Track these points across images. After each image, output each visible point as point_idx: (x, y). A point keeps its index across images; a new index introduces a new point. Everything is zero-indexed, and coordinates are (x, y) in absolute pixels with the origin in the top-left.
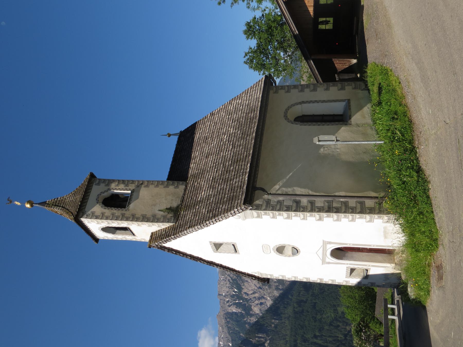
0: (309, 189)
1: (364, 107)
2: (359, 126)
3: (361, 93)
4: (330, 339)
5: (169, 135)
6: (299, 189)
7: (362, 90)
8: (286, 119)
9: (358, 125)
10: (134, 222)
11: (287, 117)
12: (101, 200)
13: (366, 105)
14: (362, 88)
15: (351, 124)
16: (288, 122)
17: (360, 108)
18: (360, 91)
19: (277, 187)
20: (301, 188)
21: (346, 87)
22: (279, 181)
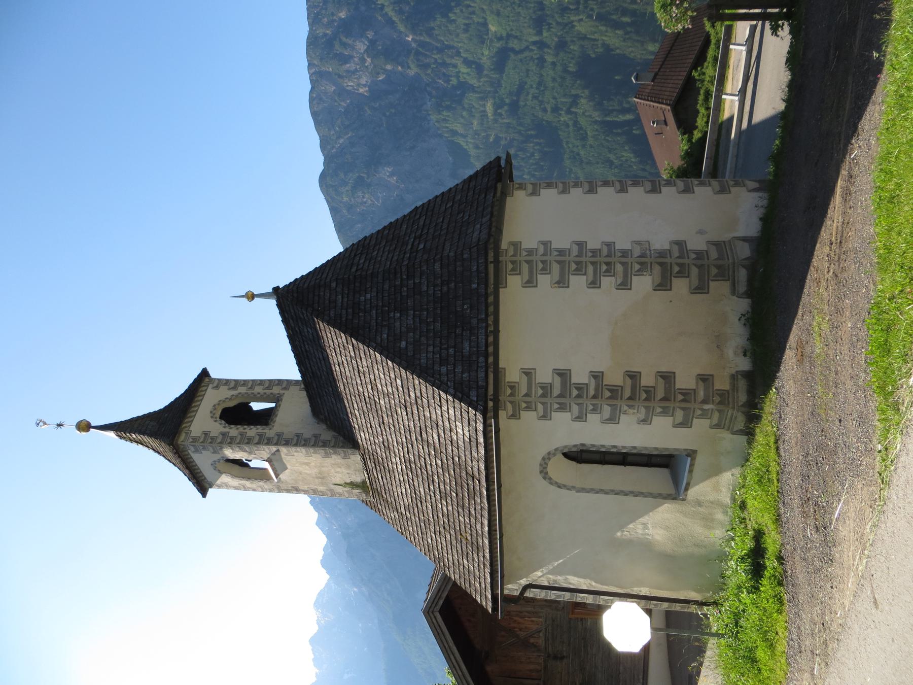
0: (591, 579)
1: (725, 471)
2: (700, 505)
3: (730, 441)
4: (626, 19)
5: (251, 296)
6: (576, 579)
7: (733, 433)
8: (545, 478)
9: (699, 503)
10: (298, 449)
11: (547, 473)
12: (218, 414)
13: (730, 469)
14: (735, 429)
15: (684, 500)
16: (551, 483)
17: (716, 471)
18: (726, 435)
19: (539, 573)
20: (578, 577)
21: (712, 284)
22: (541, 567)
